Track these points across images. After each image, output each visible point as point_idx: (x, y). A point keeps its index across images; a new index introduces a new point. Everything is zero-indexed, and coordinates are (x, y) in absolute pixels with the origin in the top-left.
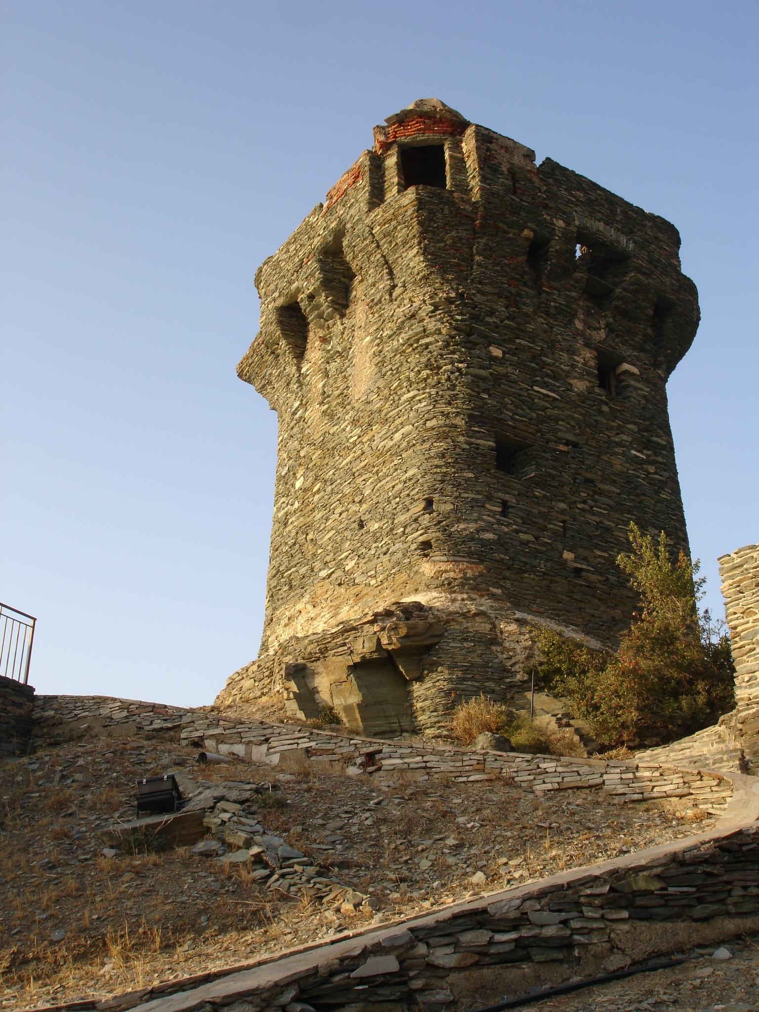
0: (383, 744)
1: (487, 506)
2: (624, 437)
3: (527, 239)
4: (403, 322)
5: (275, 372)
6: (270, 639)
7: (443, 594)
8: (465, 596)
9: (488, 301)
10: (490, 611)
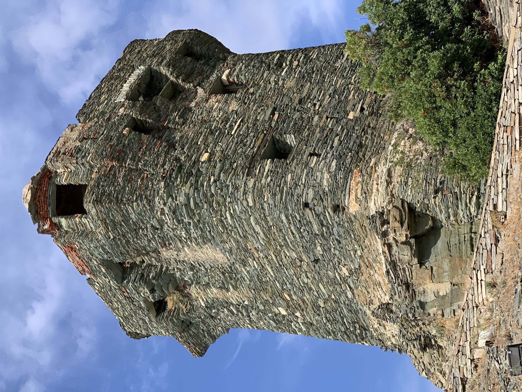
0: (486, 209)
1: (312, 166)
2: (272, 79)
3: (130, 132)
6: (394, 343)
7: (373, 198)
8: (375, 182)
9: (170, 161)
10: (387, 165)
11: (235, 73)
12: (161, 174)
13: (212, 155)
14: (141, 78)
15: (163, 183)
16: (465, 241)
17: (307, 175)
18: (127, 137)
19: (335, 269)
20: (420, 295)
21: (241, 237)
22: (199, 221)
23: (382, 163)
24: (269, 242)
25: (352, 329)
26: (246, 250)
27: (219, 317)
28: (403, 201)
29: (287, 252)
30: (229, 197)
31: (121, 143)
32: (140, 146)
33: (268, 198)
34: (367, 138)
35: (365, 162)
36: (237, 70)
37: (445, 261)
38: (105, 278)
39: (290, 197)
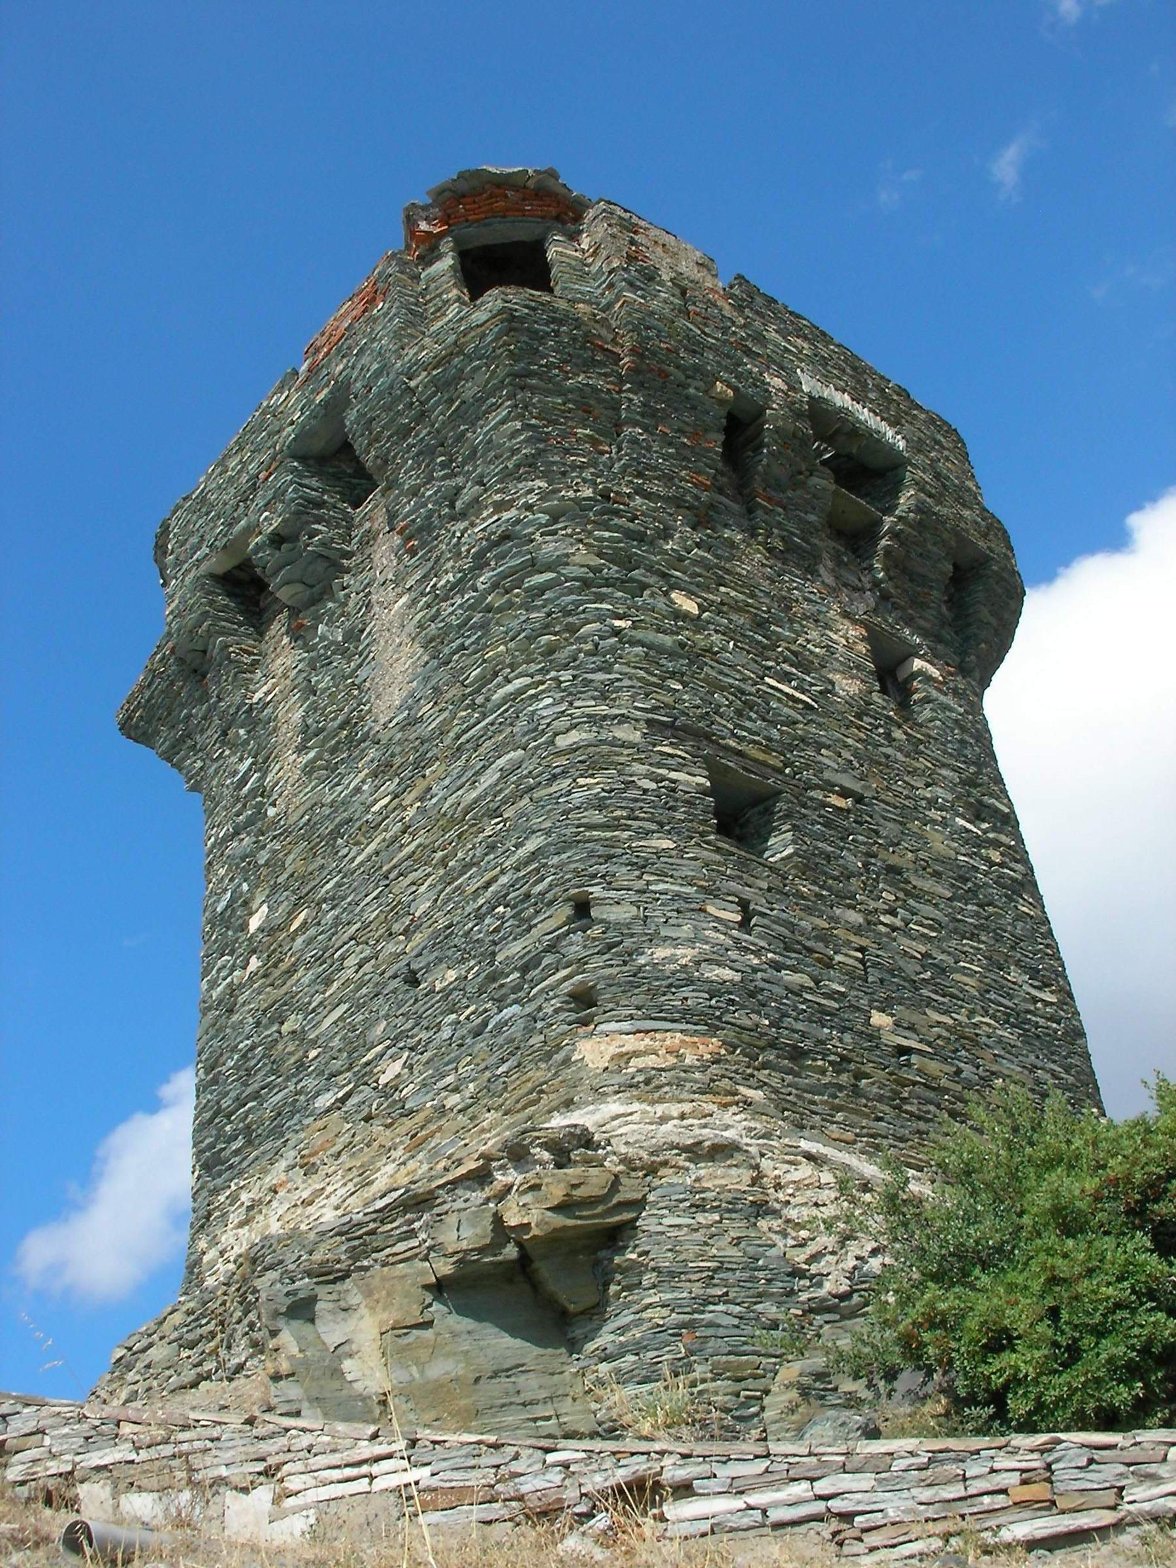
1: (710, 909)
3: (722, 402)
4: (480, 555)
5: (199, 711)
6: (206, 1258)
7: (636, 1106)
8: (687, 1107)
9: (655, 510)
10: (748, 1140)
11: (935, 693)
12: (615, 489)
13: (696, 623)
14: (872, 439)
15: (588, 493)
16: (535, 1420)
17: (677, 896)
18: (706, 392)
19: (395, 1038)
20: (334, 1296)
21: (458, 737)
22: (489, 609)
23: (752, 1124)
24: (453, 822)
25: (228, 1128)
26: (420, 765)
27: (227, 752)
28: (639, 1205)
29: (426, 884)
30: (575, 677)
31: (688, 377)
32: (687, 429)
33: (589, 787)
34: (823, 1072)
35: (749, 1071)
36: (942, 698)
37: (459, 1362)
38: (302, 409)
39: (602, 851)
